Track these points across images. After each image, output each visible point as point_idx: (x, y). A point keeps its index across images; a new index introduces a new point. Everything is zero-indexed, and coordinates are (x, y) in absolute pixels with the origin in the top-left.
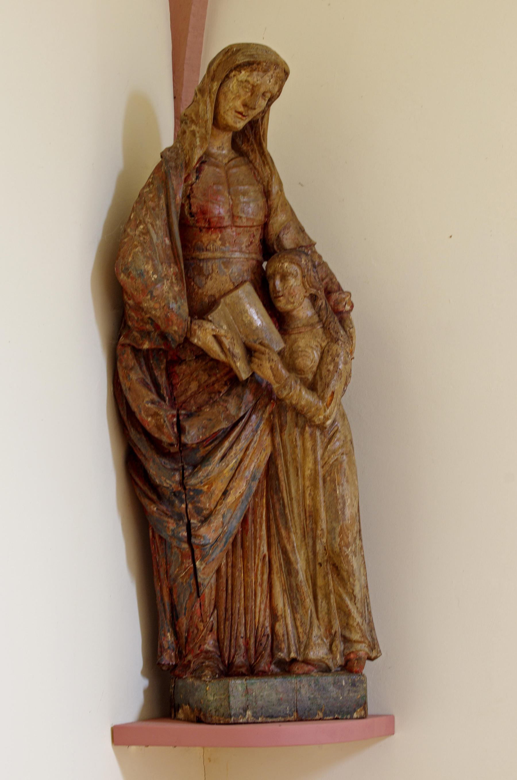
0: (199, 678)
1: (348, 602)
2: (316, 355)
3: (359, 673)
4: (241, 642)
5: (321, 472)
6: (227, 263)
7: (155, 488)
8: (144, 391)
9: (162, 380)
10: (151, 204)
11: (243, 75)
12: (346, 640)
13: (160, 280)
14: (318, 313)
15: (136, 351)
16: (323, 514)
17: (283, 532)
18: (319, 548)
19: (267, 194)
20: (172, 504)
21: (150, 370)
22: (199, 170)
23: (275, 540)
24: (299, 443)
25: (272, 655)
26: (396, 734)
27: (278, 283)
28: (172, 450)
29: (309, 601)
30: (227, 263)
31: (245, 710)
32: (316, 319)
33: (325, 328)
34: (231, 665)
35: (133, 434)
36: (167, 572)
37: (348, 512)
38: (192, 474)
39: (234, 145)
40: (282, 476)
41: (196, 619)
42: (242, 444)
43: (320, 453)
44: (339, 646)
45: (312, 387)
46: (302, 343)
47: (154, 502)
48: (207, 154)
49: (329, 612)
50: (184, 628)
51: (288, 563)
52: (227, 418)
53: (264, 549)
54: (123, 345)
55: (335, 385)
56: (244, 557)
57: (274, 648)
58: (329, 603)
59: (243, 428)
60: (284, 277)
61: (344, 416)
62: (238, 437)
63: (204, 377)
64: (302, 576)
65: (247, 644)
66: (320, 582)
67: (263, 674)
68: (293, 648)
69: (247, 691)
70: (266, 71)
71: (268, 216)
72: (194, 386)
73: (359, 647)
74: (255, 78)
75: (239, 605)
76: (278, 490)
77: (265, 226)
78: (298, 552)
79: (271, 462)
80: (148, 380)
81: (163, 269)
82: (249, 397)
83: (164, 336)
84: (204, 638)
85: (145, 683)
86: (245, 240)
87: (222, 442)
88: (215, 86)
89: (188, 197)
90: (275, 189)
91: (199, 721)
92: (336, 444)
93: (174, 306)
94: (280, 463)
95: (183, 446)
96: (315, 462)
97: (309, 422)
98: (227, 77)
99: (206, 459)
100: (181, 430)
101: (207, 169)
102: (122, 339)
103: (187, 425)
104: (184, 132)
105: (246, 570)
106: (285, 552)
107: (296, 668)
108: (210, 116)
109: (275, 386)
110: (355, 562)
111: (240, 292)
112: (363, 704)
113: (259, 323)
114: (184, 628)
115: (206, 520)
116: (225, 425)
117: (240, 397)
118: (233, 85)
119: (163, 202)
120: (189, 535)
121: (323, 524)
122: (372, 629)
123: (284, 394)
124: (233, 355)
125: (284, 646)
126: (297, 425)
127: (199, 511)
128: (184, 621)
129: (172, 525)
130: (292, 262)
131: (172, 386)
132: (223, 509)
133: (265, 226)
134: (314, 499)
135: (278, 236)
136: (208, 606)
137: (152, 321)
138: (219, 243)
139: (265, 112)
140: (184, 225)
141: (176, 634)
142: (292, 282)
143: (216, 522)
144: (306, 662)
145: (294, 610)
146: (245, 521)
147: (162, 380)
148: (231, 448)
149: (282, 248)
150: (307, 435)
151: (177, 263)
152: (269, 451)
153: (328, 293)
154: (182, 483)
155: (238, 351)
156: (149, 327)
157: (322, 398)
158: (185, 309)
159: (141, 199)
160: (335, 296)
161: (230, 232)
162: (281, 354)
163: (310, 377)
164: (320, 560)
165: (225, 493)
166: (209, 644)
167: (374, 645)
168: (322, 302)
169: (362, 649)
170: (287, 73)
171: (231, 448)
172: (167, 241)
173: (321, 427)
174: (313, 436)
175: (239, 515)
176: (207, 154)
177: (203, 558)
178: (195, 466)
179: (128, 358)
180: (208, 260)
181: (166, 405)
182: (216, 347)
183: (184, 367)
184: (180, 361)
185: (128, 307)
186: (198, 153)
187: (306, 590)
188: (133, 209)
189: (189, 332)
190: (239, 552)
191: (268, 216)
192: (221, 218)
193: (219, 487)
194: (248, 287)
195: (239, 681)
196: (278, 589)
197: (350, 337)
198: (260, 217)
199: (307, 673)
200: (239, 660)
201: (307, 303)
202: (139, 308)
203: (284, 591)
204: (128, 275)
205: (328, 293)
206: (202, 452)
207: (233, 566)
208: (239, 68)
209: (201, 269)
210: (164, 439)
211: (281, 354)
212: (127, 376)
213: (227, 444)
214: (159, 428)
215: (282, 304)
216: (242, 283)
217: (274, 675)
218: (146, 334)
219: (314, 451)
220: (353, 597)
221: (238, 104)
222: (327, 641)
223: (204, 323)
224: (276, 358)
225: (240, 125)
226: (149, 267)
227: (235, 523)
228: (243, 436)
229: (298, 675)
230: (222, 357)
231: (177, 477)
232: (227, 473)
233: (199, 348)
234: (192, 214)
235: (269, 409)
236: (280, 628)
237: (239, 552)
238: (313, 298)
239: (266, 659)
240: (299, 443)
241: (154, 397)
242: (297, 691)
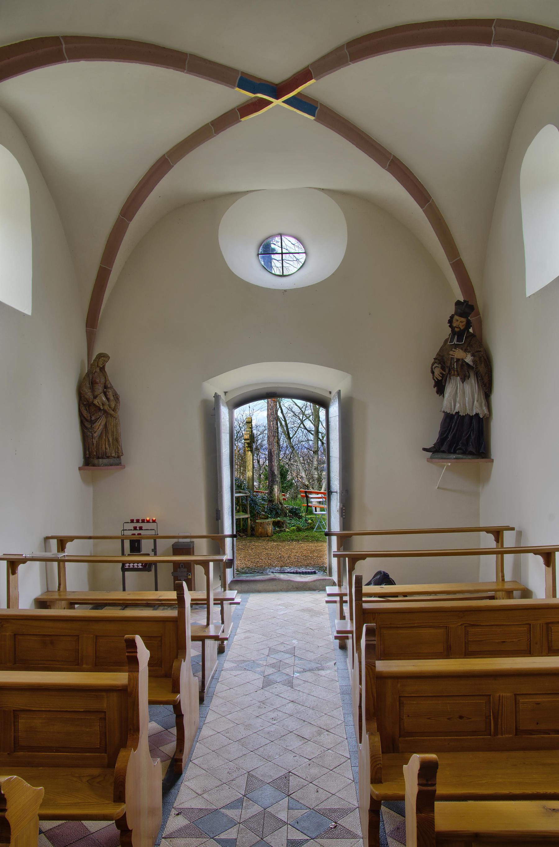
0: (93, 459)
1: (118, 446)
2: (114, 405)
3: (120, 458)
4: (100, 453)
5: (115, 424)
6: (99, 389)
7: (86, 427)
8: (84, 411)
9: (88, 409)
10: (86, 379)
11: (103, 358)
12: (118, 453)
13: (88, 392)
14: (114, 398)
15: (83, 404)
16: (115, 432)
17: (108, 435)
18: (114, 437)
19: (105, 378)
20: (89, 430)
21: (85, 407)
22: (94, 374)
23: (106, 436)
24: (111, 420)
25: (106, 455)
26: (126, 468)
27: (108, 393)
28: (89, 421)
29: (112, 446)
30: (99, 389)
31: (102, 464)
32: (114, 399)
33: (115, 401)
34: (99, 457)
35: (83, 418)
36: (88, 441)
37: (119, 432)
38: (93, 425)
39: (100, 370)
40: (108, 425)
41: (93, 449)
42: (101, 420)
43: (114, 421)
44: (117, 454)
45: (113, 411)
46: (111, 403)
47: (86, 429)
48: (96, 371)
49: (115, 448)
50: (90, 451)
51: (109, 440)
52: (99, 416)
53: (104, 437)
54: (81, 403)
55: (117, 410)
56: (101, 439)
57: (106, 454)
58: (115, 446)
59: (101, 417)
60: (109, 392)
61: (118, 416)
62: (100, 419)
63: (95, 409)
64: (111, 442)
65: (101, 453)
66: (114, 443)
67: (104, 458)
68: (109, 454)
69: (102, 461)
70: (107, 358)
71: (106, 382)
72: (93, 410)
73: (120, 454)
74: (105, 359)
75: (100, 447)
76: (107, 428)
77: (105, 383)
78: (12, 779)
79: (106, 423)
80: (85, 409)
81: (89, 390)
82: (102, 412)
83: (88, 401)
84: (94, 453)
85: (83, 460)
86: (102, 386)
87: (98, 420)
88: (98, 360)
89: (92, 378)
90: (107, 377)
91: (94, 466)
92: (117, 420)
93: (91, 397)
94: (107, 423)
95: (91, 420)
96: (114, 423)
97: (113, 416)
98: (100, 358)
99: (95, 422)
100: (91, 418)
101: (96, 373)
102: (81, 402)
103: (92, 416)
104: (92, 367)
105: (101, 442)
106: (108, 438)
107: (110, 457)
108: (96, 365)
109: (107, 410)
110: (120, 440)
111: (101, 394)
112: (121, 463)
113: (104, 400)
114: (90, 451)
115: (95, 433)
116: (99, 417)
117: (101, 412)
118: (101, 360)
119: (88, 379)
120: (92, 435)
121: (115, 434)
122: (122, 451)
123: (109, 412)
124: (100, 405)
125: (108, 454)
126: (110, 417)
127: (94, 431)
128: (90, 450)
129: (89, 433)
130: (110, 390)
131: (89, 410)
132: (98, 431)
133: (105, 383)
134: (113, 429)
135: (254, 535)
136: (95, 446)
137: (86, 399)
138: (97, 386)
139: (105, 364)
140: (92, 383)
141: (89, 452)
142: (110, 393)
143: (97, 433)
144: (112, 456)
145: (109, 448)
146: (101, 433)
147: (88, 409)
148: (99, 421)
149: (108, 387)
150: (112, 419)
151: (91, 389)
152: (106, 421)
153: (116, 395)
154: (91, 426)
155: (101, 404)
156: (85, 400)
157: (115, 413)
158: (92, 397)
159: (84, 378)
160: (117, 396)
161: (100, 384)
162: (108, 405)
163: (113, 409)
164: (114, 439)
165: (98, 428)
166: (95, 454)
167: (122, 454)
168: (115, 396)
169: (121, 454)
170: (110, 358)
171: (99, 421)
172: (89, 386)
173: (115, 417)
174: (113, 418)
175: (100, 432)
176: (96, 371)
177: (94, 439)
178: (93, 423)
179: (82, 405)
180: (95, 389)
181: (88, 413)
182: (98, 404)
183: (91, 407)
184: (90, 406)
185: (311, 418)
186: (94, 371)
187: (112, 444)
188: (83, 380)
189: (93, 401)
190: (100, 438)
191: (106, 382)
192: (98, 382)
193: (97, 427)
194: (103, 394)
195: (101, 460)
196: (107, 444)
197: (120, 402)
198: (104, 382)
199: (112, 458)
200: (100, 456)
201: (112, 396)
202: (84, 396)
203: (108, 445)
204: (83, 391)
205: (116, 395)
206: (94, 421)
207: (99, 440)
208: (102, 357)
209: (94, 390)
210: (88, 419)
211: (108, 405)
212: (82, 408)
213: (99, 420)
214: (87, 417)
215: (108, 397)
216: (102, 393)
217: (106, 458)
218: (85, 401)
219: (113, 421)
220: (119, 446)
221: (101, 363)
222: (115, 453)
223: (96, 400)
224: (107, 406)
225: (102, 366)
226: (86, 390)
227: (100, 433)
228: (100, 421)
229: (110, 458)
230: (98, 405)
231: (90, 425)
232: (99, 425)
233: (94, 404)
234: (93, 381)
235: (106, 414)
236: (107, 451)
237: (100, 438)
238: (113, 396)
239: (105, 456)
240: (111, 420)
241: (86, 412)
242: (110, 461)
